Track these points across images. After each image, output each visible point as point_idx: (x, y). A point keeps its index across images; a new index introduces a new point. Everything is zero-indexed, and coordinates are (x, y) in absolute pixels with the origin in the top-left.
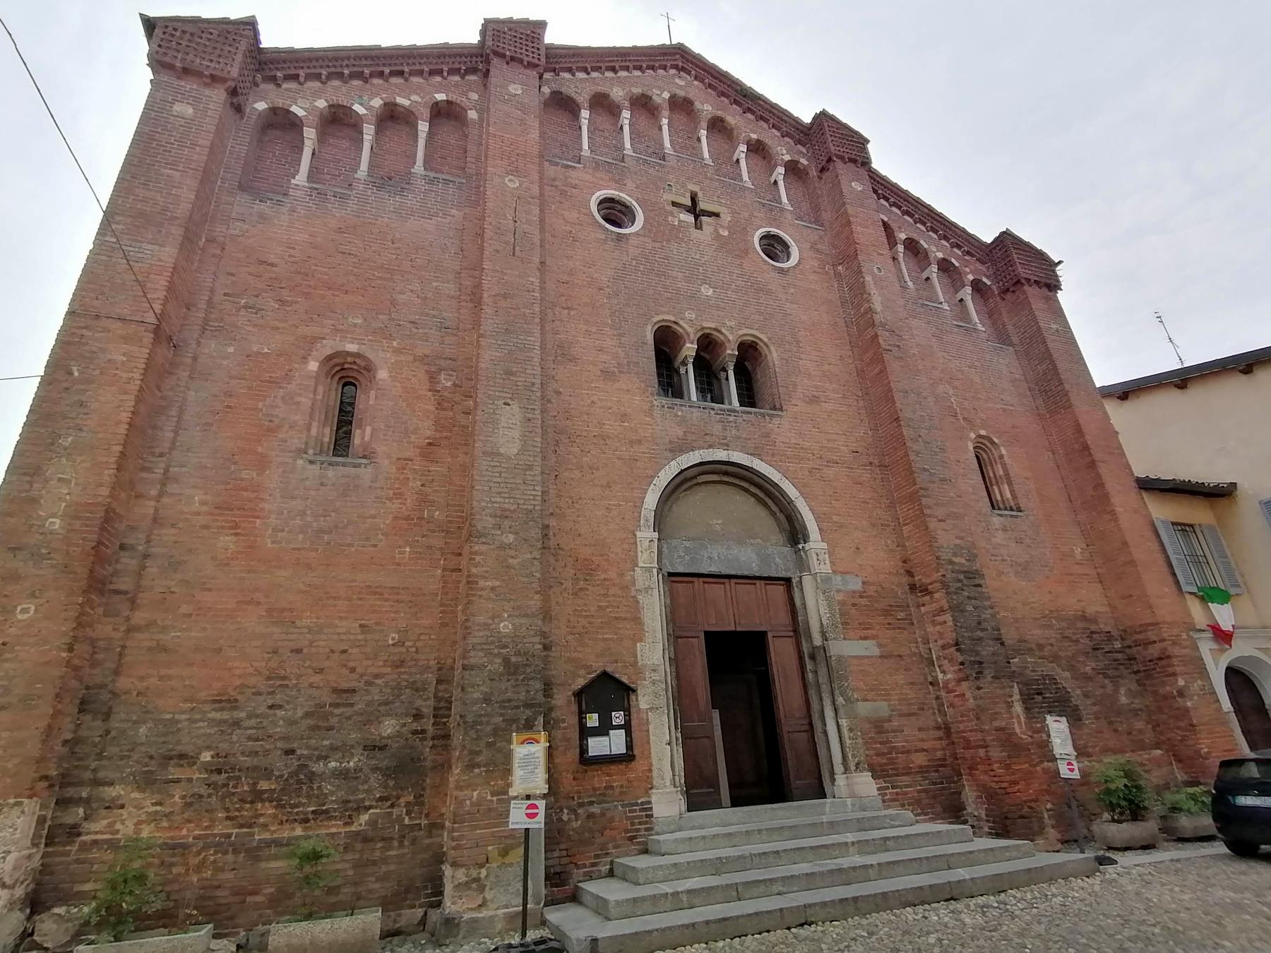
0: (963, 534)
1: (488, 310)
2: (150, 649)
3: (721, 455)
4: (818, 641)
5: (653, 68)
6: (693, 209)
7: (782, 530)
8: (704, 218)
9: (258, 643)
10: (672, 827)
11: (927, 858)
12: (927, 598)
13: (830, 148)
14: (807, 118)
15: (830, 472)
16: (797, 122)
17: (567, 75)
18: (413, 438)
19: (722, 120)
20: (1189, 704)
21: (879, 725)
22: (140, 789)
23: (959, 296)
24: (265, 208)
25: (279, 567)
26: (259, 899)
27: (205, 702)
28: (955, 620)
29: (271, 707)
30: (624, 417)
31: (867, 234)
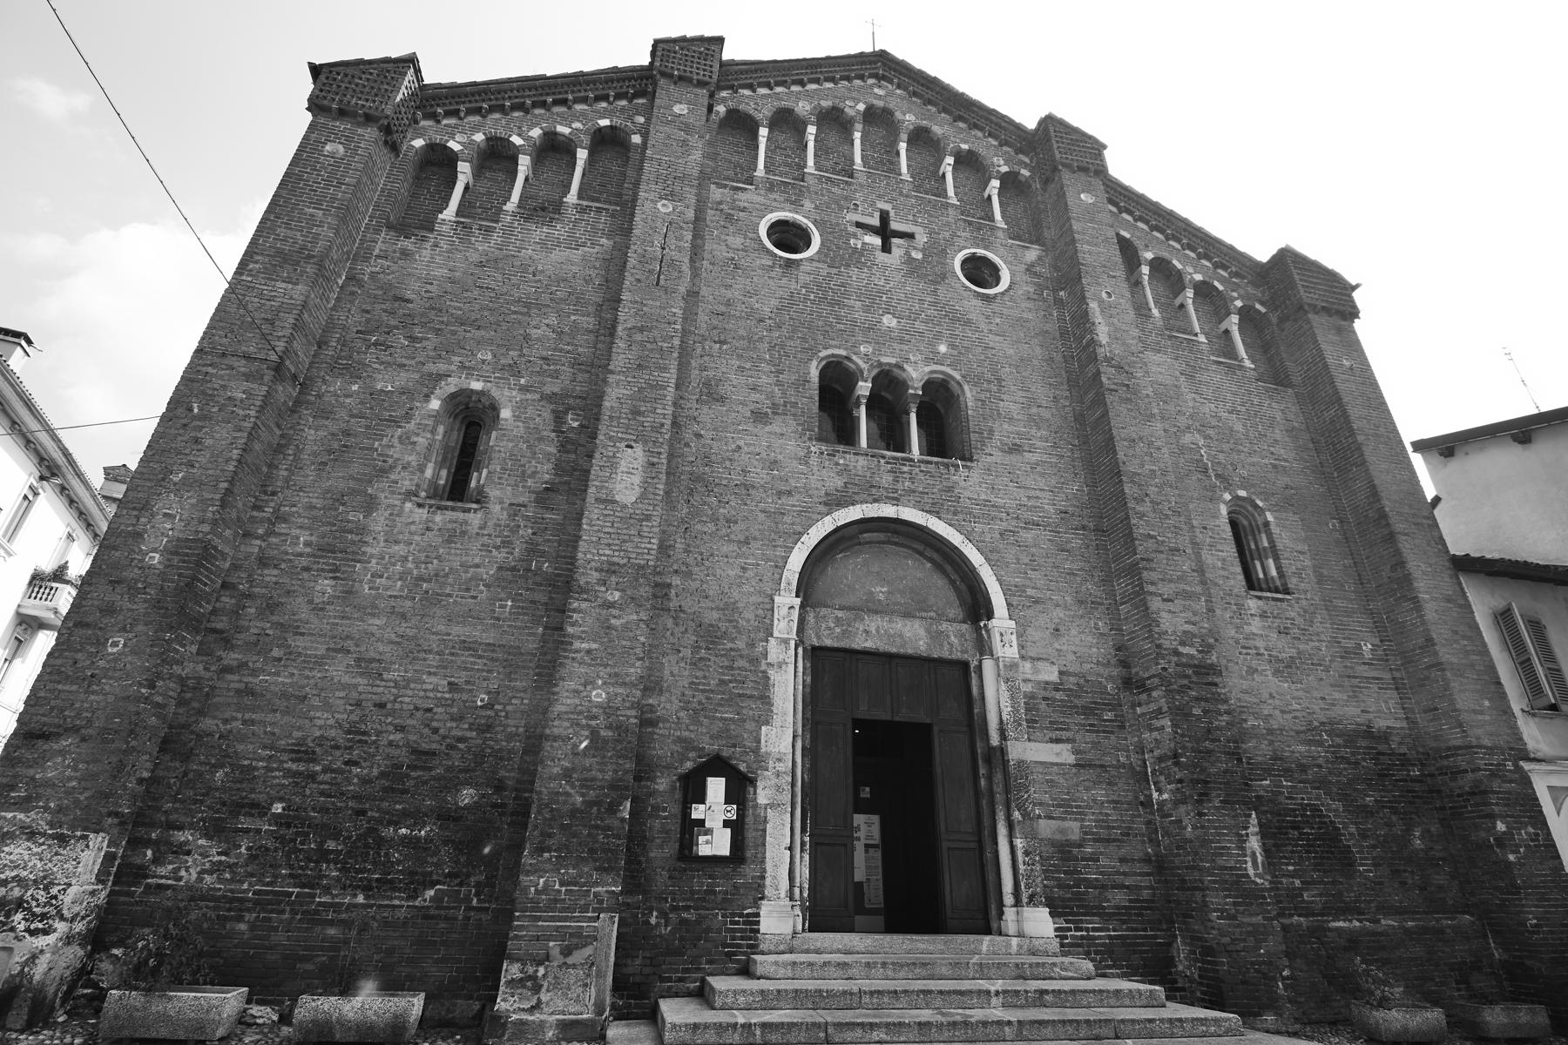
0: (1197, 619)
1: (621, 344)
2: (238, 691)
3: (888, 511)
4: (995, 740)
5: (848, 79)
6: (885, 232)
7: (962, 603)
8: (895, 241)
9: (342, 694)
10: (782, 947)
11: (1087, 1021)
12: (1144, 696)
13: (1056, 156)
14: (1031, 124)
15: (1028, 536)
16: (1019, 128)
17: (747, 92)
18: (530, 482)
19: (926, 130)
20: (1511, 857)
21: (1064, 850)
22: (208, 837)
23: (1223, 326)
24: (408, 244)
25: (373, 615)
26: (309, 967)
27: (284, 751)
28: (1174, 726)
29: (346, 763)
30: (774, 464)
31: (1097, 251)
